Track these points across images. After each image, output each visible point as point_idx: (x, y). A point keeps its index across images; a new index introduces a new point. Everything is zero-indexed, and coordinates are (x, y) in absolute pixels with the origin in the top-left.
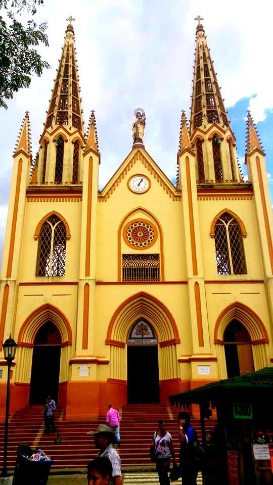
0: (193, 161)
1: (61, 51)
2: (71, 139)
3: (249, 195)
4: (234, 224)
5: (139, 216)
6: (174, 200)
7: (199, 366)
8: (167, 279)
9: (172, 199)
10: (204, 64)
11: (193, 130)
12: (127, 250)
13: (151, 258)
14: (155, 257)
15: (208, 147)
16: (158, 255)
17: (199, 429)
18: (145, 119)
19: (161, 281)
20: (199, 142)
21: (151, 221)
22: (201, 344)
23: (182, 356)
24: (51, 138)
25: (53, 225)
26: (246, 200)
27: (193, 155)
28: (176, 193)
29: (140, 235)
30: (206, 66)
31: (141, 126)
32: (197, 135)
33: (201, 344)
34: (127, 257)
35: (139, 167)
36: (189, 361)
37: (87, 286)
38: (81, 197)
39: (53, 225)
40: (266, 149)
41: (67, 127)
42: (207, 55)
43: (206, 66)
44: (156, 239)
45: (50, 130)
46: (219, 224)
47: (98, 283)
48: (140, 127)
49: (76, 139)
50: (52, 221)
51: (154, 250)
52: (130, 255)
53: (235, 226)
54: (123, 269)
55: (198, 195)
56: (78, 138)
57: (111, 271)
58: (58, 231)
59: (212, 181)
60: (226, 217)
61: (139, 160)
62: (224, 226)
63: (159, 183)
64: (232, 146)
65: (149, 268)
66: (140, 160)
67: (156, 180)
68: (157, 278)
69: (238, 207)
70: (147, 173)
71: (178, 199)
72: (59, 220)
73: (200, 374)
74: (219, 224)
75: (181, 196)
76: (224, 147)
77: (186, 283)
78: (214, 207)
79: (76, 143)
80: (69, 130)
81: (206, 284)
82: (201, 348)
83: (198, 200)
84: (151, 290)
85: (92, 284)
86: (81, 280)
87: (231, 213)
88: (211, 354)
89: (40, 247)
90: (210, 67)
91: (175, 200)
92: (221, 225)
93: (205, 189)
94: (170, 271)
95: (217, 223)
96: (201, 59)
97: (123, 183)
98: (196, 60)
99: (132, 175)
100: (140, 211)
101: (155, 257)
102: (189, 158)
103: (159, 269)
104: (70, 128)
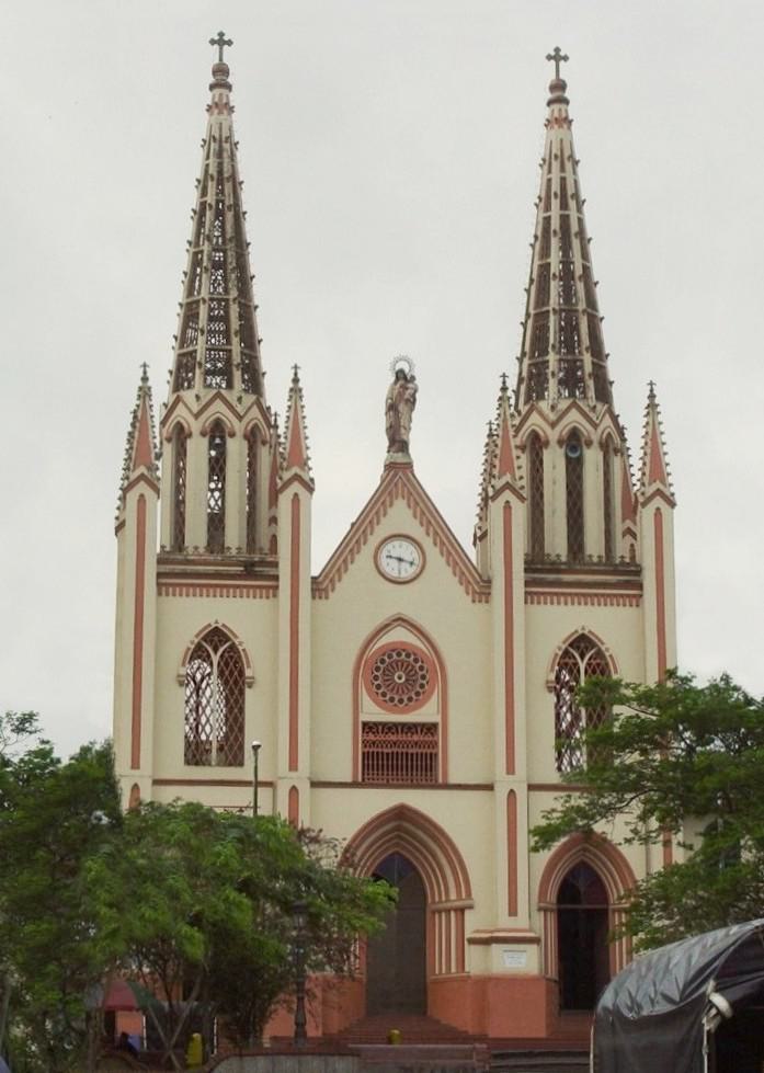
0: (520, 512)
1: (201, 153)
2: (239, 427)
3: (634, 596)
4: (598, 661)
5: (399, 635)
6: (474, 601)
7: (506, 951)
8: (453, 780)
9: (470, 598)
10: (561, 216)
11: (526, 403)
12: (373, 712)
13: (422, 731)
14: (430, 728)
15: (555, 462)
16: (435, 725)
17: (620, 917)
18: (416, 391)
19: (440, 781)
20: (536, 444)
21: (424, 649)
22: (513, 911)
23: (478, 931)
24: (195, 426)
25: (216, 651)
26: (634, 607)
27: (522, 499)
28: (481, 589)
29: (400, 678)
30: (565, 220)
31: (406, 408)
32: (533, 424)
33: (513, 911)
34: (370, 728)
35: (400, 516)
36: (487, 942)
37: (294, 792)
38: (277, 587)
39: (216, 651)
40: (678, 499)
41: (232, 397)
42: (570, 190)
43: (565, 220)
44: (383, 646)
45: (188, 396)
46: (567, 660)
47: (315, 784)
48: (402, 407)
49: (251, 425)
50: (212, 641)
51: (427, 713)
52: (376, 724)
53: (598, 665)
54: (363, 754)
55: (526, 593)
56: (255, 421)
57: (341, 759)
58: (227, 664)
59: (558, 556)
60: (582, 645)
61: (400, 498)
62: (576, 664)
63: (457, 579)
64: (611, 452)
65: (422, 754)
66: (403, 497)
67: (437, 550)
68: (431, 775)
69: (608, 623)
70: (417, 531)
71: (484, 599)
72: (228, 639)
73: (508, 965)
74: (567, 660)
75: (489, 594)
76: (592, 458)
77: (489, 787)
78: (560, 620)
79: (252, 438)
80: (234, 403)
81: (532, 793)
82: (513, 918)
83: (526, 602)
84: (418, 799)
85: (305, 791)
86: (280, 778)
87: (593, 638)
88: (530, 930)
89: (240, 719)
90: (574, 228)
91: (477, 600)
92: (571, 661)
93: (542, 573)
94: (461, 761)
95: (563, 657)
96: (555, 232)
97: (367, 551)
98: (543, 196)
99: (416, 582)
100: (399, 622)
101: (429, 729)
102: (512, 504)
103: (436, 755)
104: (240, 399)
